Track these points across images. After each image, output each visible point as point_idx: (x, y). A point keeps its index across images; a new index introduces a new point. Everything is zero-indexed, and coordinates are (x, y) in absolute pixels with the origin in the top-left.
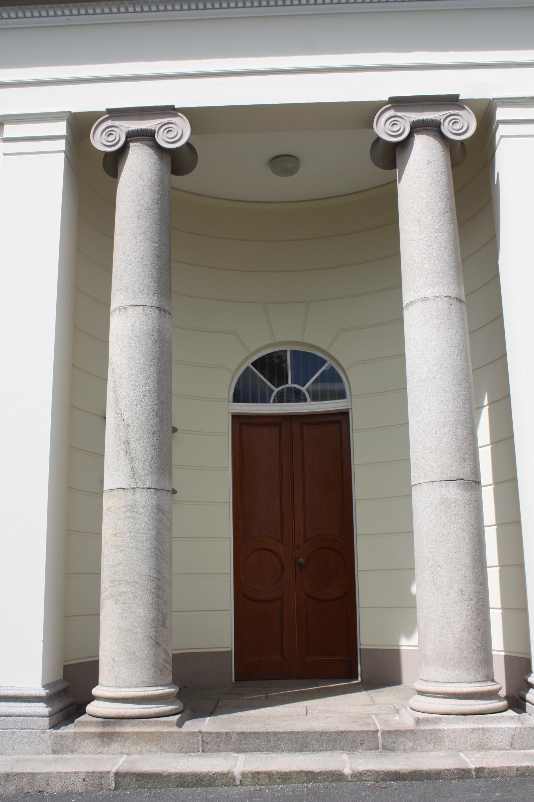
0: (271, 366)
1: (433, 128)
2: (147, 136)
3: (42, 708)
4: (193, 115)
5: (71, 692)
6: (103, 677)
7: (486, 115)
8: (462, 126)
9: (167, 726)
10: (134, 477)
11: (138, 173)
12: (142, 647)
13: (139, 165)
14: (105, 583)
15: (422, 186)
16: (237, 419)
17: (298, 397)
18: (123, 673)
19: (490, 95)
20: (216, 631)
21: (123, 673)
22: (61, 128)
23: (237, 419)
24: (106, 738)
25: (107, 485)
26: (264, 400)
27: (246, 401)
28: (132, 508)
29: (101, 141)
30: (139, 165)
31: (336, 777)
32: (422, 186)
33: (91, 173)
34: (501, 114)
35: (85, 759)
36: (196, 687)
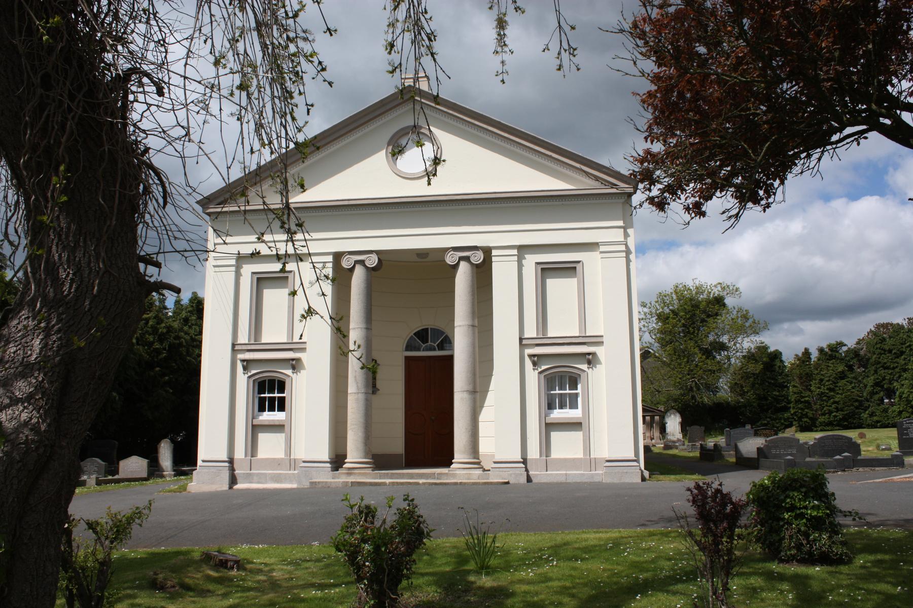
0: (422, 335)
1: (467, 259)
2: (362, 262)
3: (328, 465)
4: (378, 252)
5: (338, 461)
6: (348, 456)
7: (487, 252)
8: (478, 257)
9: (369, 471)
10: (358, 389)
11: (359, 275)
12: (361, 446)
13: (359, 273)
14: (349, 425)
15: (463, 279)
16: (407, 358)
17: (432, 349)
18: (354, 454)
19: (491, 245)
20: (398, 446)
21: (354, 454)
22: (330, 258)
23: (407, 358)
24: (349, 474)
25: (349, 391)
26: (419, 350)
27: (411, 350)
28: (357, 399)
29: (346, 263)
30: (359, 273)
31: (418, 484)
32: (463, 279)
33: (341, 278)
34: (494, 252)
35: (341, 478)
36: (381, 462)
